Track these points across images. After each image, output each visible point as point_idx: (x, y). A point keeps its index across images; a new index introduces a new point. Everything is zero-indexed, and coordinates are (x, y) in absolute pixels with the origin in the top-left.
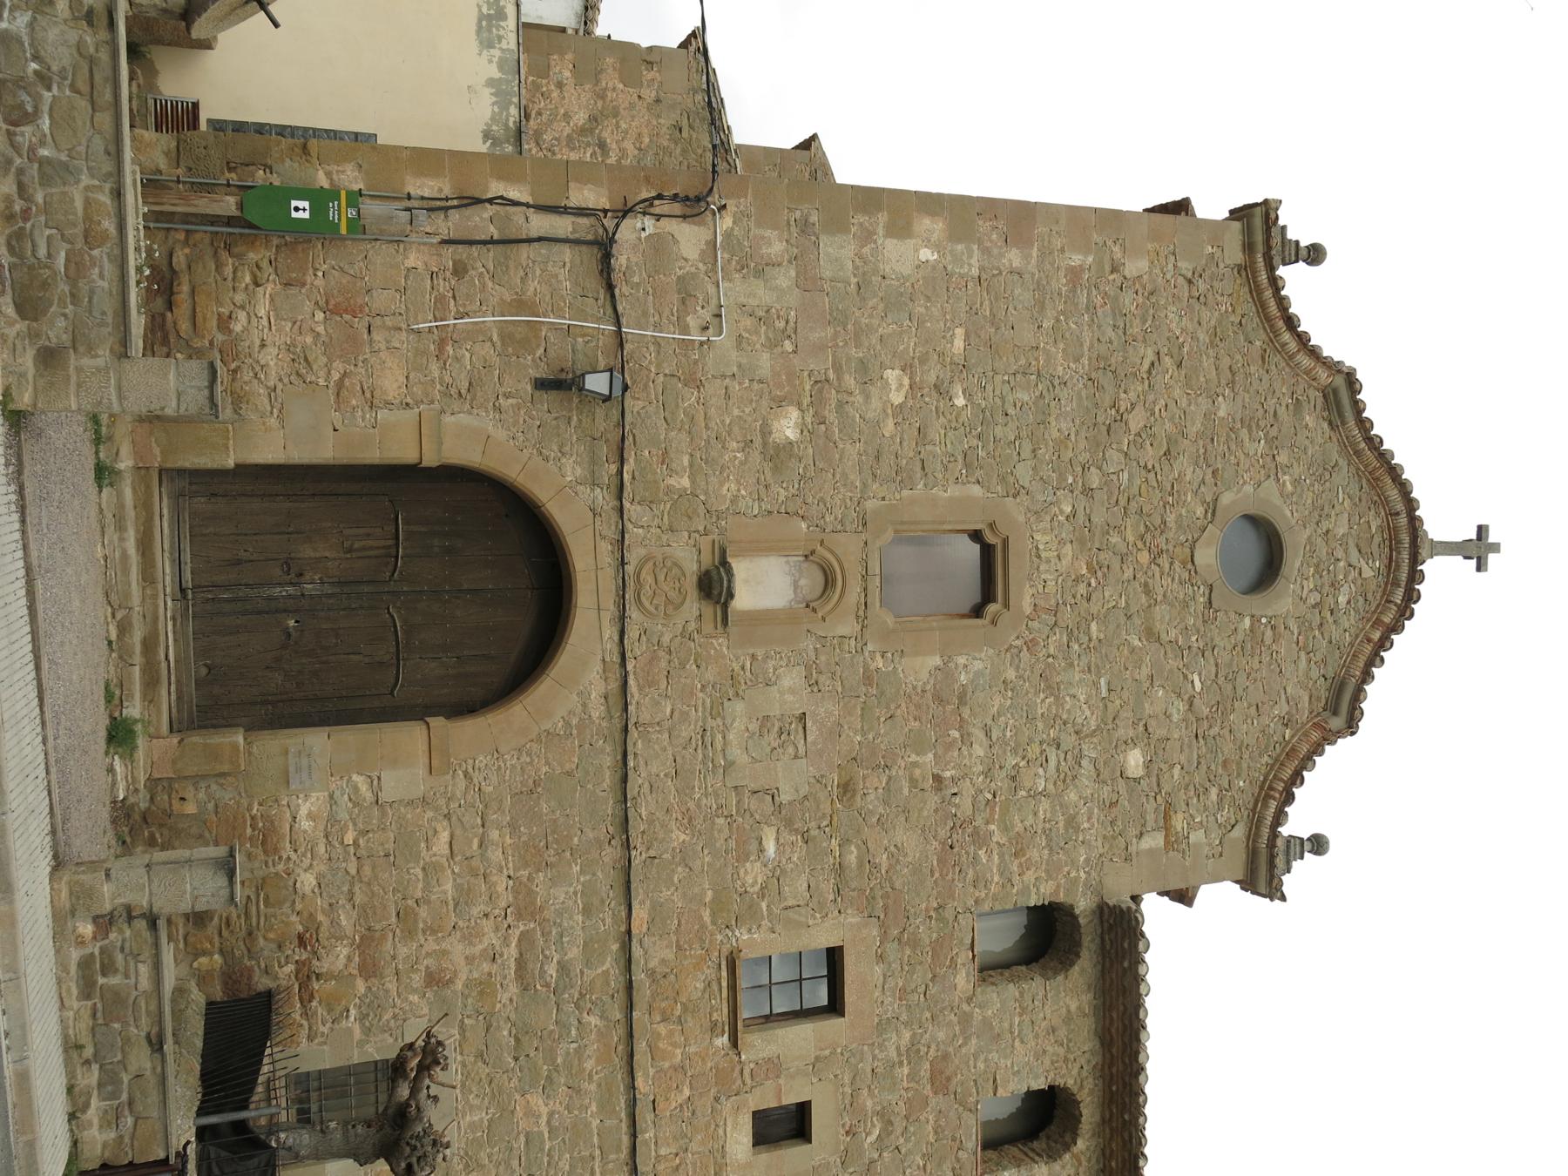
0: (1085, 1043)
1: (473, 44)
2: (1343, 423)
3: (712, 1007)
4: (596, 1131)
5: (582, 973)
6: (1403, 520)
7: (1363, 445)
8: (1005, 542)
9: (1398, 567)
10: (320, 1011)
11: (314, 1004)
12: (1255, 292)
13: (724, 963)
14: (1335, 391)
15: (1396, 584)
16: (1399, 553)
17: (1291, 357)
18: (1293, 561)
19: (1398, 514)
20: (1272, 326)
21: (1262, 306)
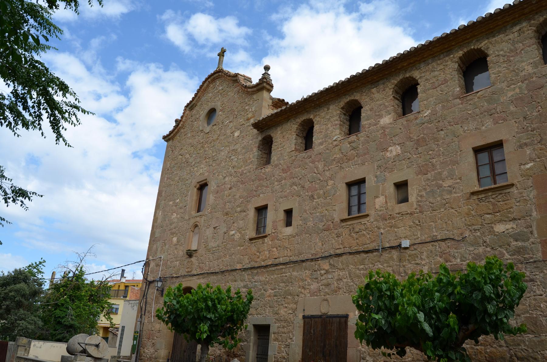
0: (513, 34)
2: (195, 104)
3: (259, 244)
4: (277, 276)
5: (246, 282)
6: (209, 80)
7: (197, 97)
8: (198, 183)
9: (217, 76)
10: (240, 352)
11: (238, 354)
12: (175, 135)
13: (251, 242)
14: (190, 108)
15: (219, 75)
16: (215, 78)
17: (184, 122)
18: (206, 111)
19: (209, 81)
20: (179, 129)
21: (177, 133)
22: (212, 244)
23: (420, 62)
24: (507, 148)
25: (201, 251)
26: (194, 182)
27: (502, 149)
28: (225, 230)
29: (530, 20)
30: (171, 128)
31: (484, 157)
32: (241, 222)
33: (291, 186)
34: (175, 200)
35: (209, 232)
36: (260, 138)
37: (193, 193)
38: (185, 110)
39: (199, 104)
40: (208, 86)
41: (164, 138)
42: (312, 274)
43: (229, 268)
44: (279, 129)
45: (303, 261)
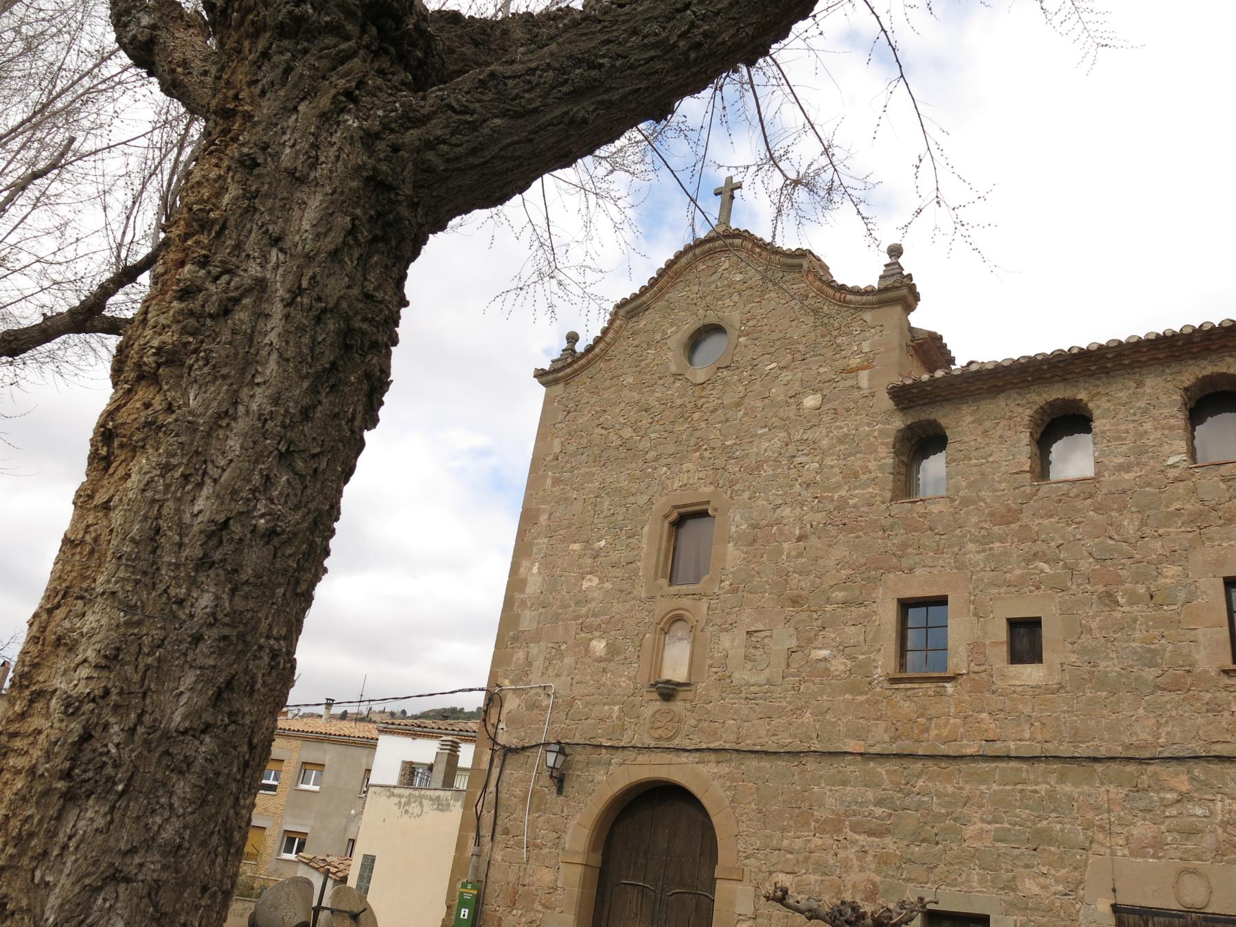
1: (447, 814)
6: (697, 251)
8: (676, 507)
15: (732, 245)
40: (689, 265)
41: (540, 375)
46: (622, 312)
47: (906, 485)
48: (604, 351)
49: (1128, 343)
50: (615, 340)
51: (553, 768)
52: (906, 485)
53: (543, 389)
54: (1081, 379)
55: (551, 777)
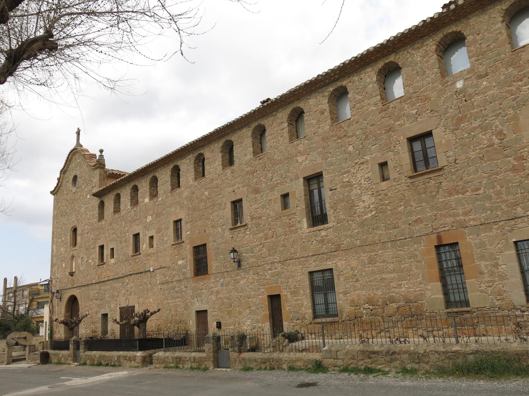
6: (72, 153)
8: (72, 227)
22: (81, 268)
23: (158, 168)
24: (183, 222)
25: (77, 273)
26: (70, 227)
27: (431, 138)
28: (86, 259)
29: (193, 153)
30: (55, 185)
31: (417, 146)
32: (93, 255)
33: (113, 235)
34: (61, 239)
35: (79, 260)
36: (99, 202)
37: (69, 234)
38: (61, 174)
39: (68, 170)
40: (72, 157)
41: (51, 192)
42: (122, 285)
43: (90, 283)
44: (107, 197)
45: (119, 278)
46: (62, 173)
47: (335, 117)
48: (61, 185)
49: (133, 173)
50: (62, 181)
51: (234, 258)
52: (335, 117)
53: (53, 196)
54: (313, 93)
55: (234, 262)
